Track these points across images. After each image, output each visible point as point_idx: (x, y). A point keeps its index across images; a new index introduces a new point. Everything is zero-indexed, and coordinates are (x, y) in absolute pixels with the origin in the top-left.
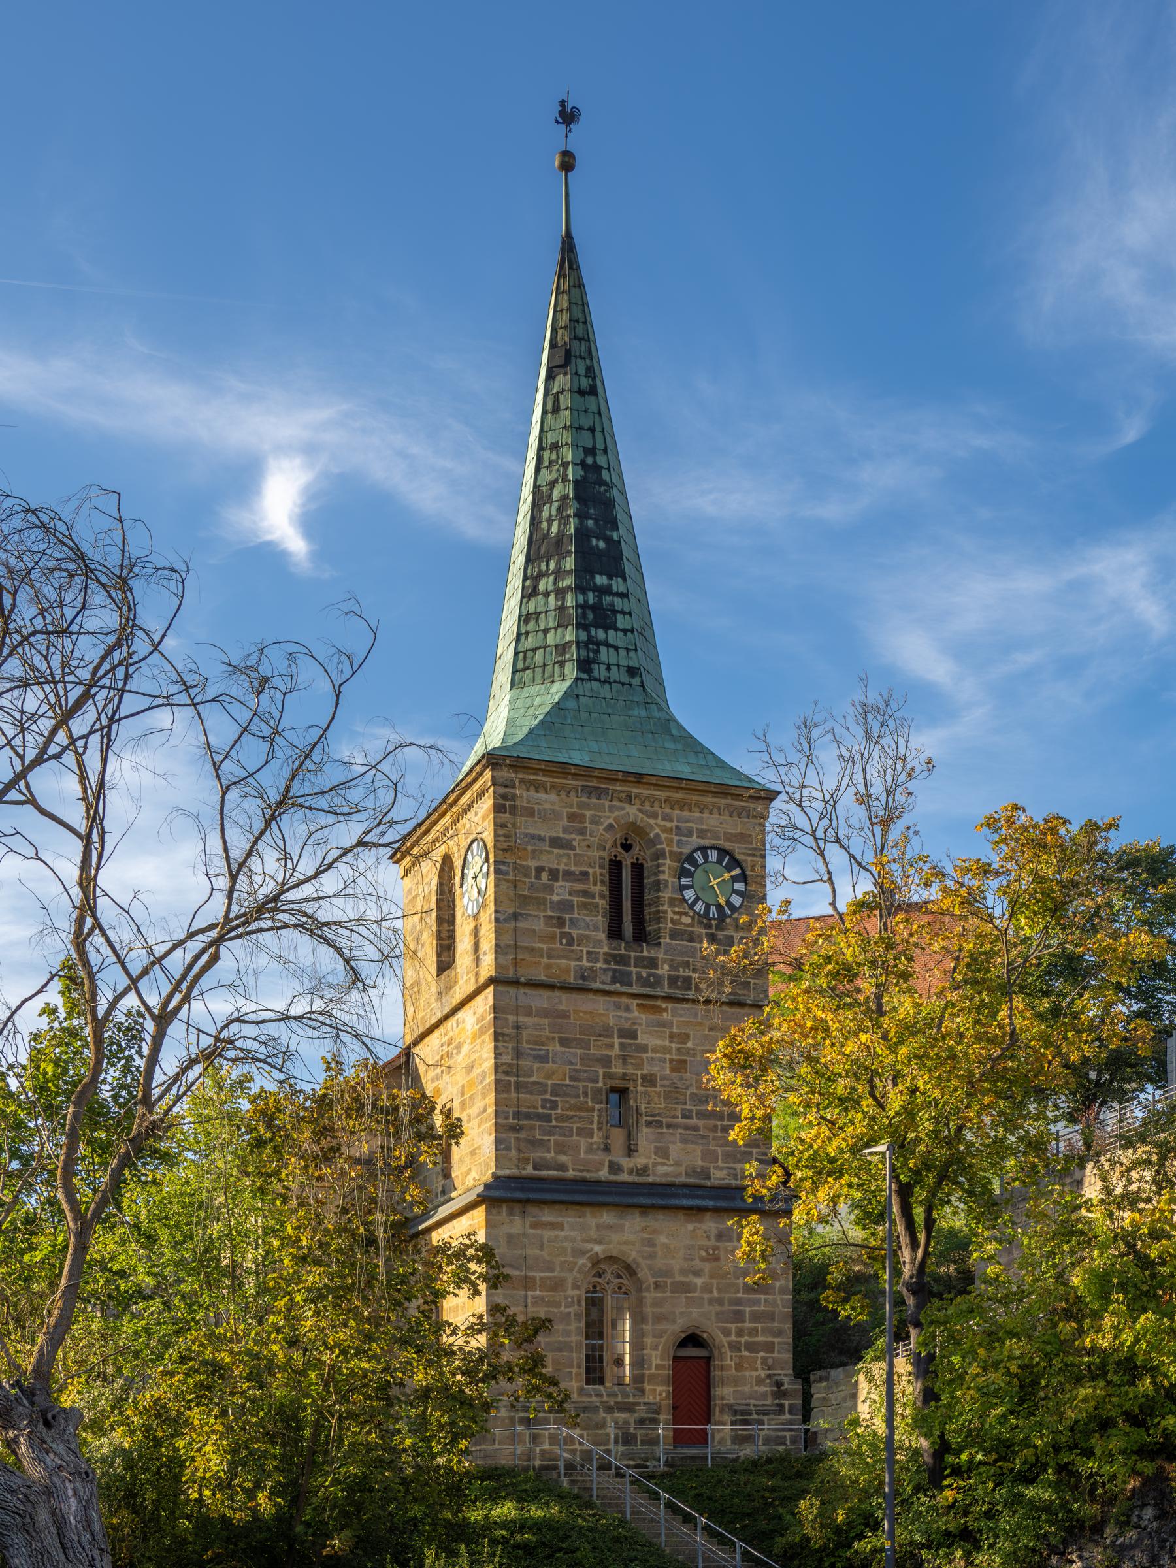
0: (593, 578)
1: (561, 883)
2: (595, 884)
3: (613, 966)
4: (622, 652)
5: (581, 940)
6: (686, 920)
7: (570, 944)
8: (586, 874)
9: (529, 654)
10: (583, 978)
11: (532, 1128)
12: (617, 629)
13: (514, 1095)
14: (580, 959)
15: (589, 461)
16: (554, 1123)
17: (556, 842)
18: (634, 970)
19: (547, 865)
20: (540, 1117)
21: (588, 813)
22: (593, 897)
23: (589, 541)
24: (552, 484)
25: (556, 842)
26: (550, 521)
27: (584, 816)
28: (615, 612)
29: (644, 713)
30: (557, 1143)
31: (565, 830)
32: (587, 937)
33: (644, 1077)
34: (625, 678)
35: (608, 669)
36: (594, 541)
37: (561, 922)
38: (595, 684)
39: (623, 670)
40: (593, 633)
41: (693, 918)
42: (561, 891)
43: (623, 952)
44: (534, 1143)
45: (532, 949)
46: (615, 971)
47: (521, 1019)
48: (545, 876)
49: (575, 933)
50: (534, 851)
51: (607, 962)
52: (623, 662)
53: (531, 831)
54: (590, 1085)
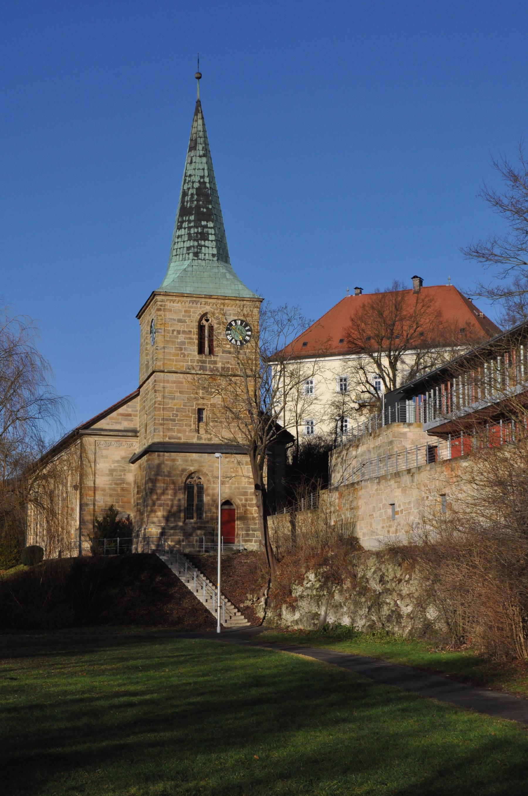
0: (201, 222)
1: (181, 335)
2: (194, 335)
3: (200, 364)
4: (210, 249)
5: (188, 355)
6: (228, 346)
7: (184, 357)
8: (191, 331)
9: (178, 250)
10: (189, 369)
11: (168, 424)
12: (209, 240)
13: (162, 412)
14: (188, 362)
15: (202, 180)
16: (177, 422)
17: (180, 321)
18: (208, 365)
19: (176, 329)
20: (171, 420)
21: (192, 310)
22: (193, 339)
23: (200, 209)
24: (189, 189)
25: (180, 321)
26: (187, 202)
27: (190, 311)
28: (208, 234)
29: (217, 271)
30: (177, 429)
31: (183, 316)
32: (191, 354)
33: (211, 404)
34: (211, 258)
35: (205, 255)
36: (202, 209)
37: (181, 349)
38: (200, 261)
39: (210, 255)
40: (200, 242)
41: (231, 346)
42: (181, 338)
43: (204, 359)
44: (169, 430)
45: (170, 359)
46: (200, 366)
47: (166, 384)
48: (175, 333)
49: (186, 353)
50: (171, 324)
51: (198, 363)
52: (211, 252)
53: (171, 317)
54: (191, 408)
